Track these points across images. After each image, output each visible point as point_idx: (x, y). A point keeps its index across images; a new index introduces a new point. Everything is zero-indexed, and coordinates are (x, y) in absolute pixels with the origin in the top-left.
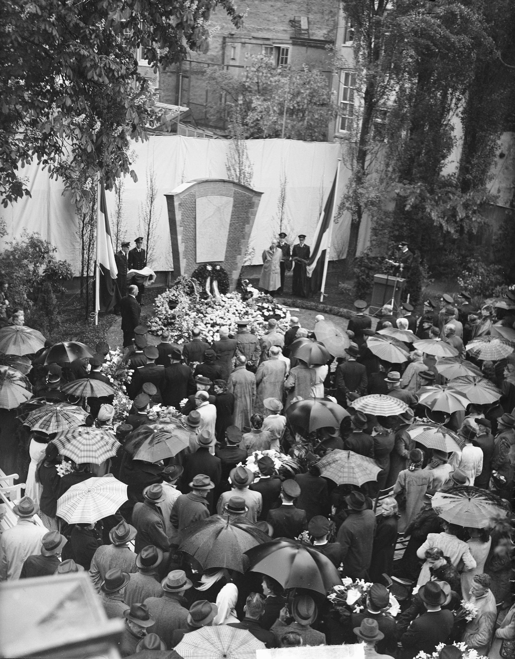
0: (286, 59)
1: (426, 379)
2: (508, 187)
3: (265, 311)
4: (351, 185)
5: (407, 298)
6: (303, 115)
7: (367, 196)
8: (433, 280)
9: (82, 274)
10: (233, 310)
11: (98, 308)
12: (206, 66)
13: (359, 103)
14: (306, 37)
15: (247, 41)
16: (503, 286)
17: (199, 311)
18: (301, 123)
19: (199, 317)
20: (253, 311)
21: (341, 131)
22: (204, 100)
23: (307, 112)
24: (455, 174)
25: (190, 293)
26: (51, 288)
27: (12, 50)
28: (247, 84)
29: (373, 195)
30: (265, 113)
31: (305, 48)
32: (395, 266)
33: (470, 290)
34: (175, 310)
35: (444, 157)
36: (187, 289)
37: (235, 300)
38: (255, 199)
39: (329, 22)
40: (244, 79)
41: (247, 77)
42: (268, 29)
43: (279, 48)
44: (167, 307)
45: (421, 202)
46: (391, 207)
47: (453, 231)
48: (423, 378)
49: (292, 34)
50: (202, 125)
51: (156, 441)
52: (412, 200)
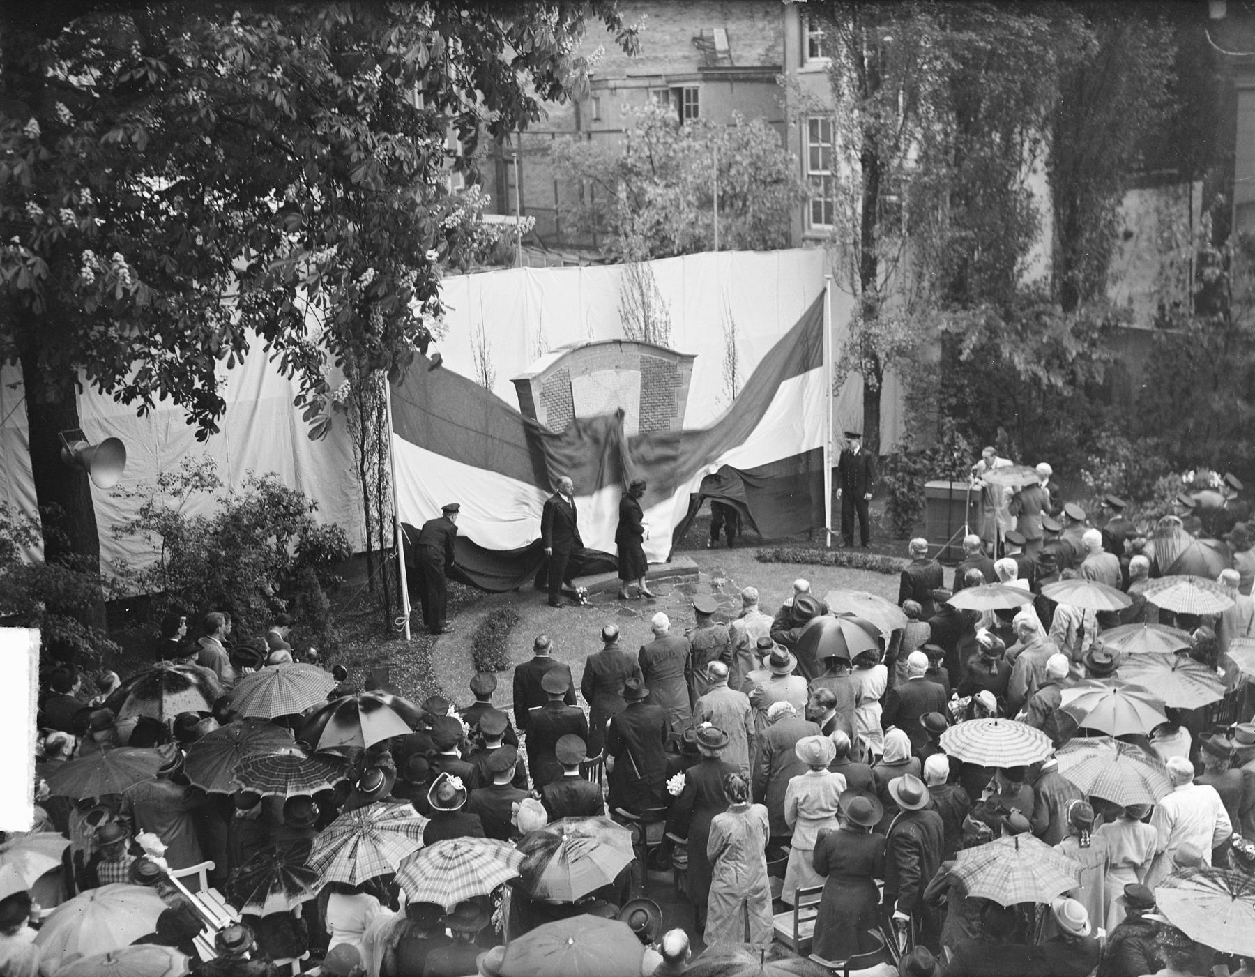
0: (696, 108)
2: (1147, 290)
6: (744, 205)
9: (369, 546)
11: (407, 608)
12: (550, 137)
13: (850, 171)
14: (727, 64)
15: (619, 83)
16: (1170, 477)
18: (742, 219)
21: (815, 226)
22: (553, 200)
23: (750, 198)
24: (1046, 278)
26: (316, 581)
27: (78, 182)
28: (629, 161)
31: (727, 85)
35: (1024, 249)
38: (681, 370)
39: (766, 33)
42: (656, 58)
43: (679, 91)
45: (990, 338)
46: (935, 354)
47: (1060, 384)
49: (700, 61)
50: (554, 246)
51: (571, 857)
52: (972, 340)
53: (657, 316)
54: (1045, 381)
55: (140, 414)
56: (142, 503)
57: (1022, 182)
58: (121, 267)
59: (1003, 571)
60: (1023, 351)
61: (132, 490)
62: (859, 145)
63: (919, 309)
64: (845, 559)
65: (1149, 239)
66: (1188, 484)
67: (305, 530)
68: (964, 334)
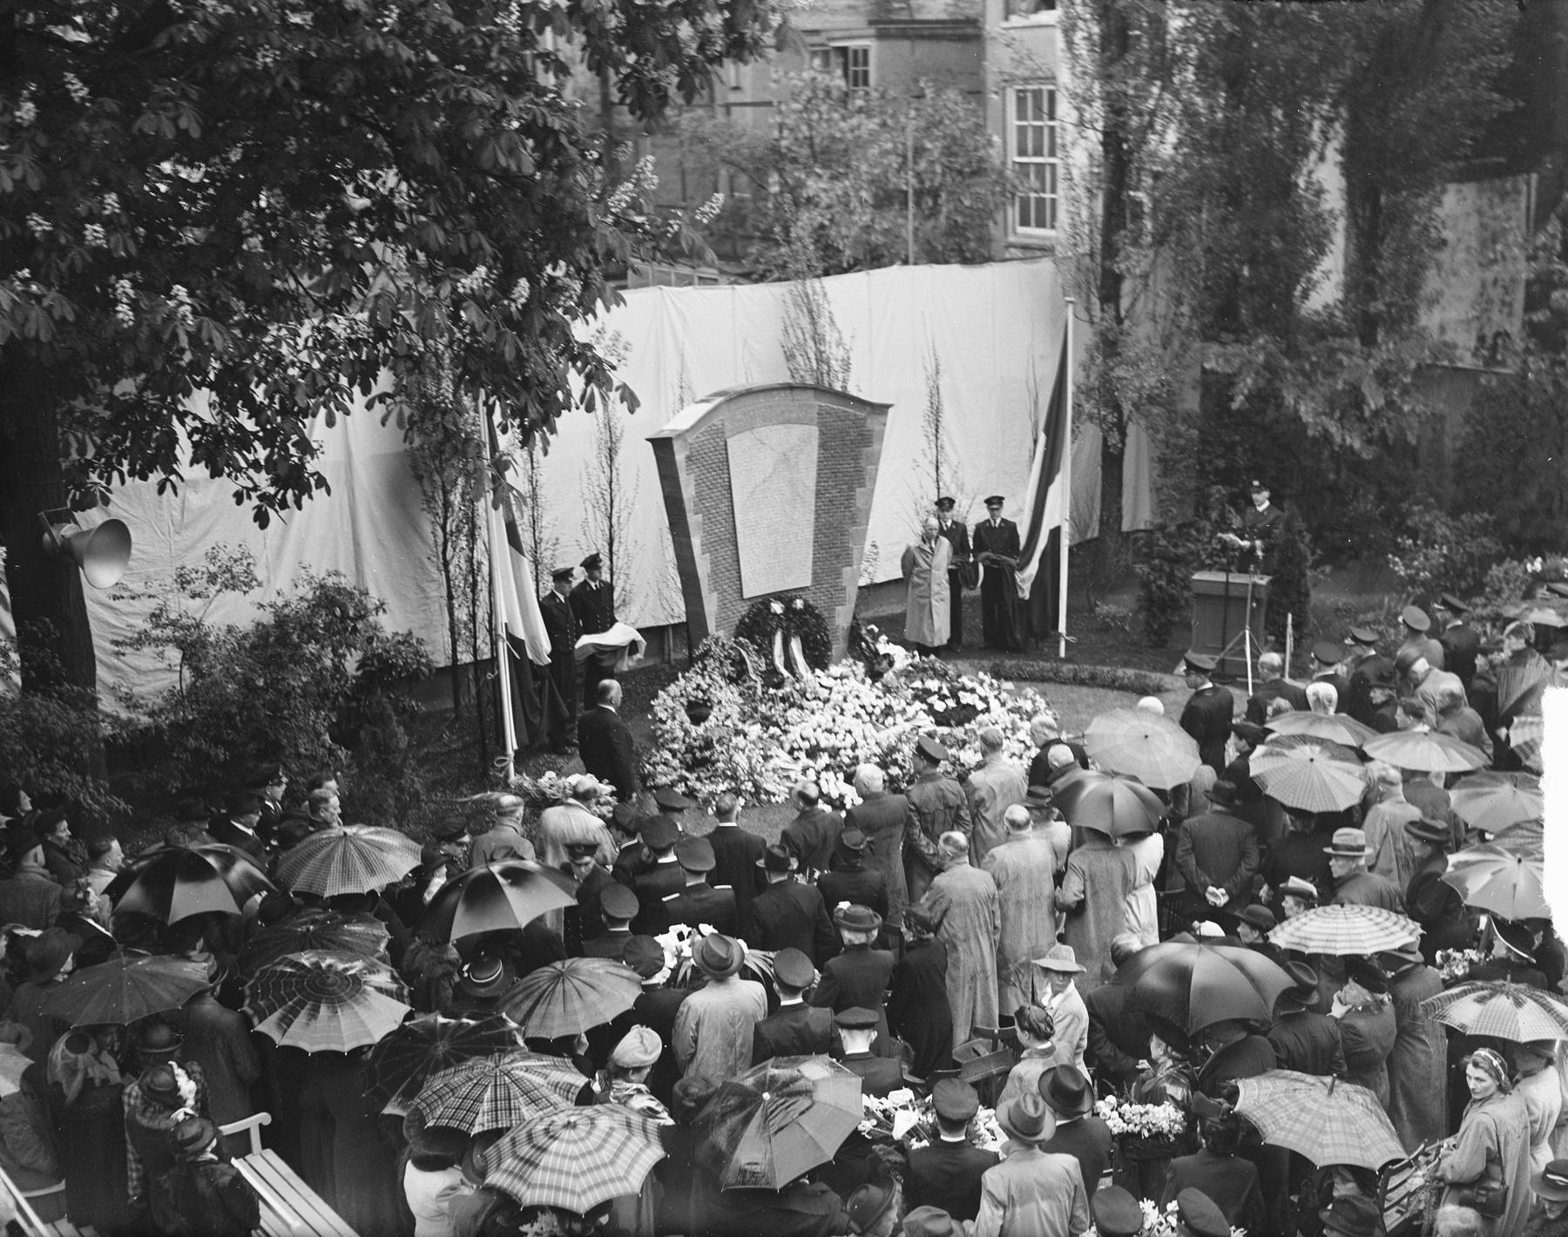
0: (866, 73)
1: (1429, 842)
2: (1463, 317)
3: (933, 699)
4: (1092, 358)
5: (1285, 626)
6: (935, 203)
7: (1137, 384)
8: (1328, 569)
10: (851, 706)
11: (512, 744)
14: (904, 16)
16: (1506, 565)
17: (767, 722)
18: (930, 224)
19: (772, 737)
20: (903, 703)
21: (1021, 230)
23: (944, 195)
25: (738, 676)
26: (390, 710)
28: (784, 143)
29: (1151, 381)
30: (838, 208)
31: (906, 44)
32: (1241, 548)
33: (1424, 584)
34: (707, 724)
35: (1310, 265)
36: (729, 669)
37: (852, 683)
38: (872, 423)
40: (776, 134)
41: (781, 127)
43: (843, 51)
44: (686, 719)
45: (1269, 382)
46: (1191, 401)
47: (1357, 445)
48: (1416, 837)
51: (776, 1122)
52: (1248, 383)
53: (834, 353)
54: (1338, 439)
55: (161, 491)
56: (151, 605)
57: (1310, 173)
58: (182, 303)
59: (1318, 700)
60: (1313, 398)
61: (138, 587)
62: (1100, 125)
63: (1176, 344)
64: (1085, 675)
65: (1468, 249)
66: (1534, 574)
67: (370, 640)
68: (1235, 375)
